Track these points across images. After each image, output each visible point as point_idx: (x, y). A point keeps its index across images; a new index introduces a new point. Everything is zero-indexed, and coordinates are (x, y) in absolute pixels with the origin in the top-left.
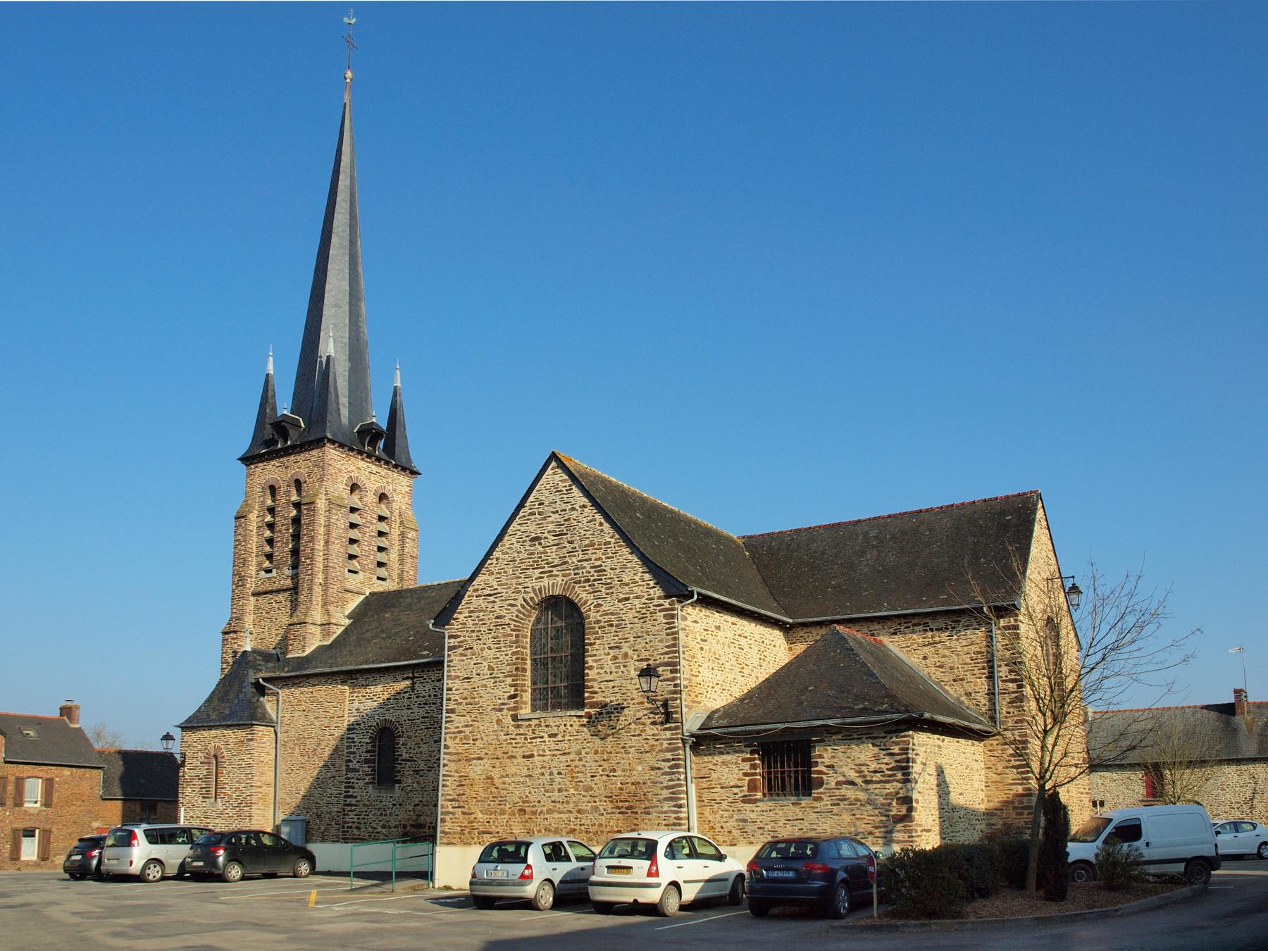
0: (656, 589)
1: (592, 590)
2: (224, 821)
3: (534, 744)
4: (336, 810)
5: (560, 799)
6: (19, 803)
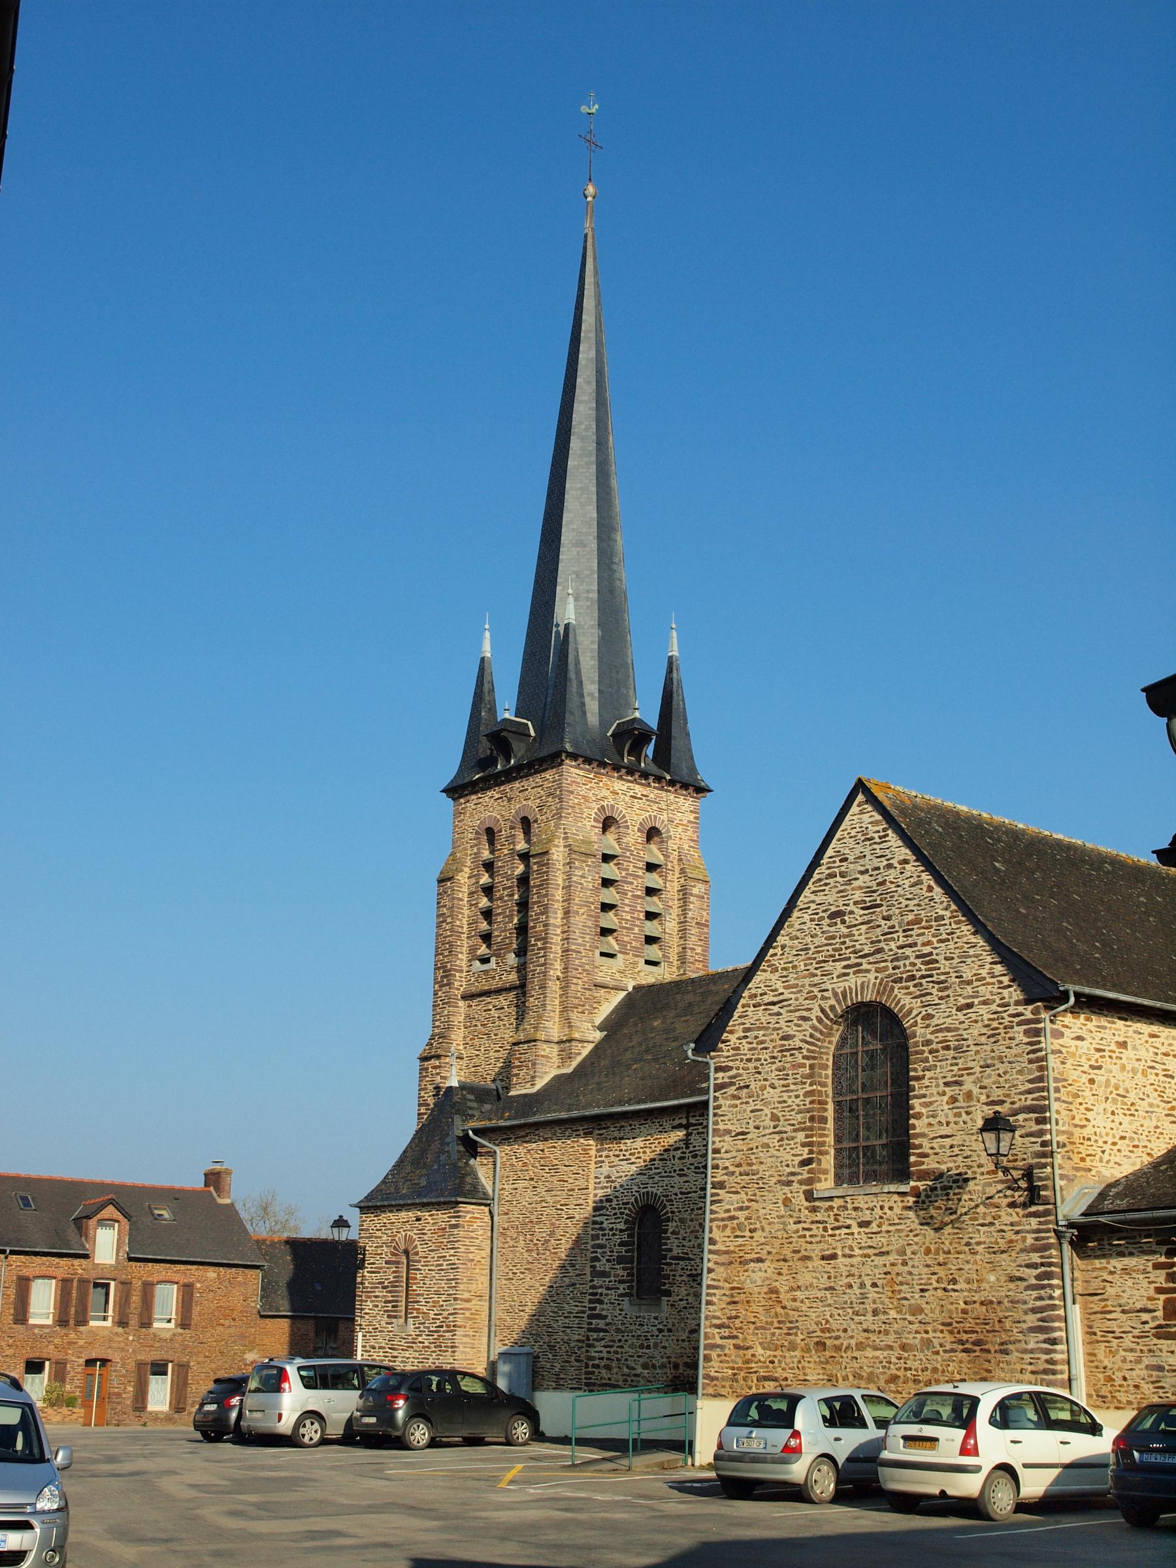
0: (1011, 989)
1: (918, 993)
2: (417, 1354)
3: (837, 1238)
4: (577, 1337)
5: (875, 1327)
6: (146, 1323)
